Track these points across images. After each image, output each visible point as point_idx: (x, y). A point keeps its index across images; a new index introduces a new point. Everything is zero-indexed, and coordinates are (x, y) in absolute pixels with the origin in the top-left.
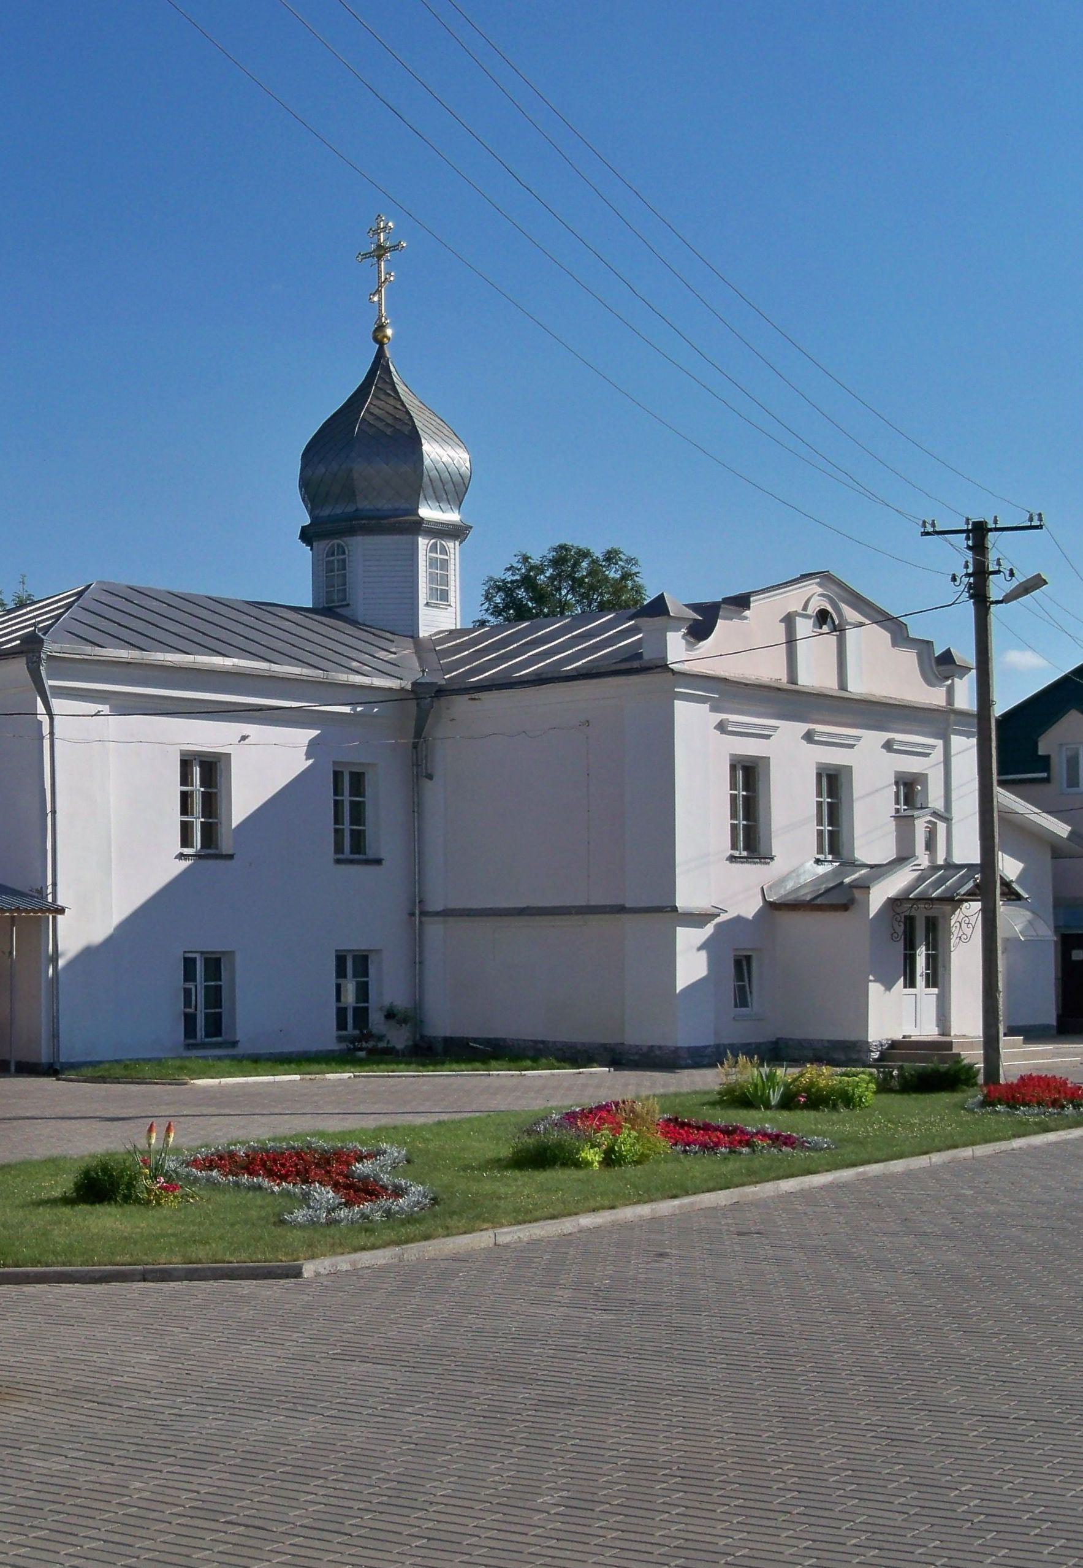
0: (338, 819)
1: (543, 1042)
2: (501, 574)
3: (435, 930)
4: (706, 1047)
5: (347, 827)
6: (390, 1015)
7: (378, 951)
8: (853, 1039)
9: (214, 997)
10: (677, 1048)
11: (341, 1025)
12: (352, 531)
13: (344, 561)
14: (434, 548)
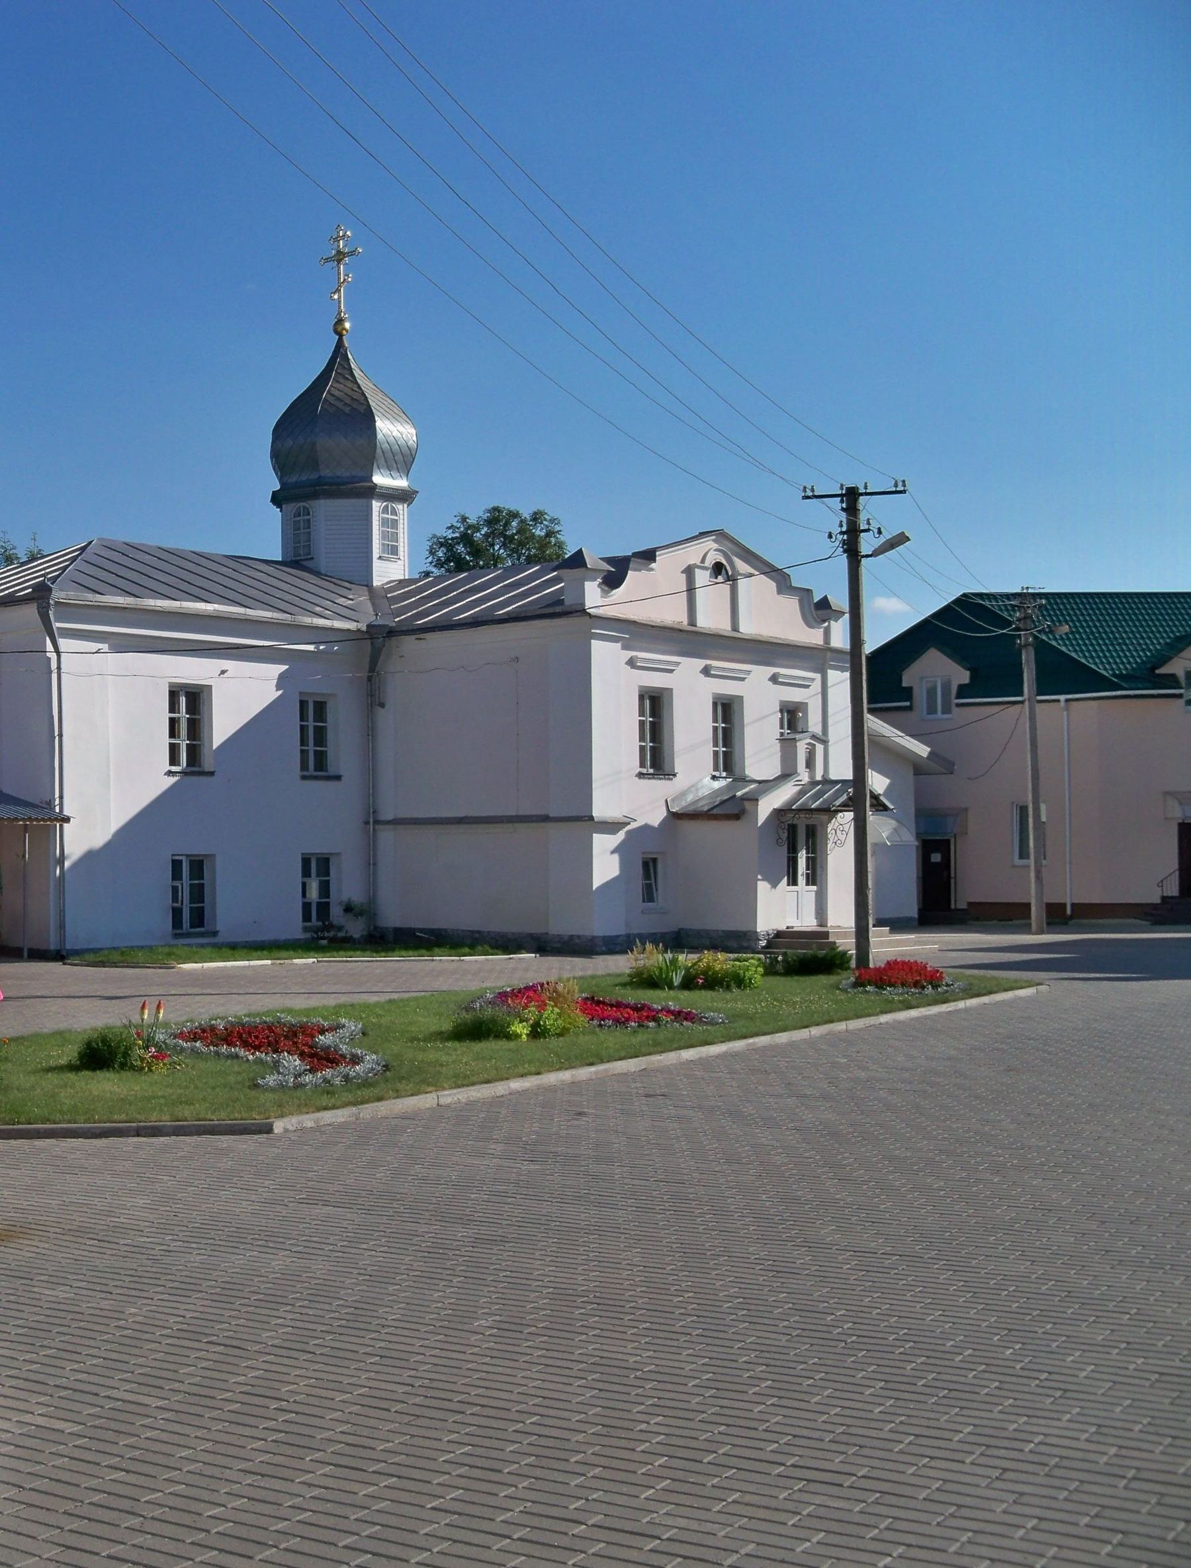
0: (303, 741)
1: (479, 932)
3: (386, 837)
4: (618, 936)
5: (311, 748)
6: (348, 909)
8: (744, 929)
9: (198, 893)
10: (594, 938)
11: (307, 917)
12: (315, 496)
13: (309, 521)
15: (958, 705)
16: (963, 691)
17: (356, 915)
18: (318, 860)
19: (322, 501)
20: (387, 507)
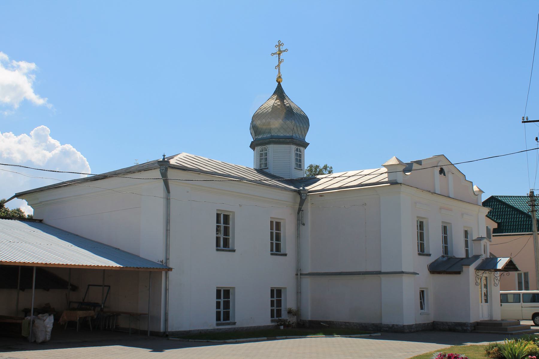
0: (272, 239)
1: (348, 323)
2: (313, 164)
3: (307, 282)
4: (413, 325)
5: (274, 242)
6: (290, 312)
7: (285, 288)
8: (464, 322)
9: (227, 305)
10: (404, 326)
11: (272, 316)
12: (269, 143)
13: (266, 153)
14: (297, 150)
15: (493, 236)
16: (495, 231)
17: (294, 315)
18: (224, 290)
19: (272, 145)
20: (297, 149)
